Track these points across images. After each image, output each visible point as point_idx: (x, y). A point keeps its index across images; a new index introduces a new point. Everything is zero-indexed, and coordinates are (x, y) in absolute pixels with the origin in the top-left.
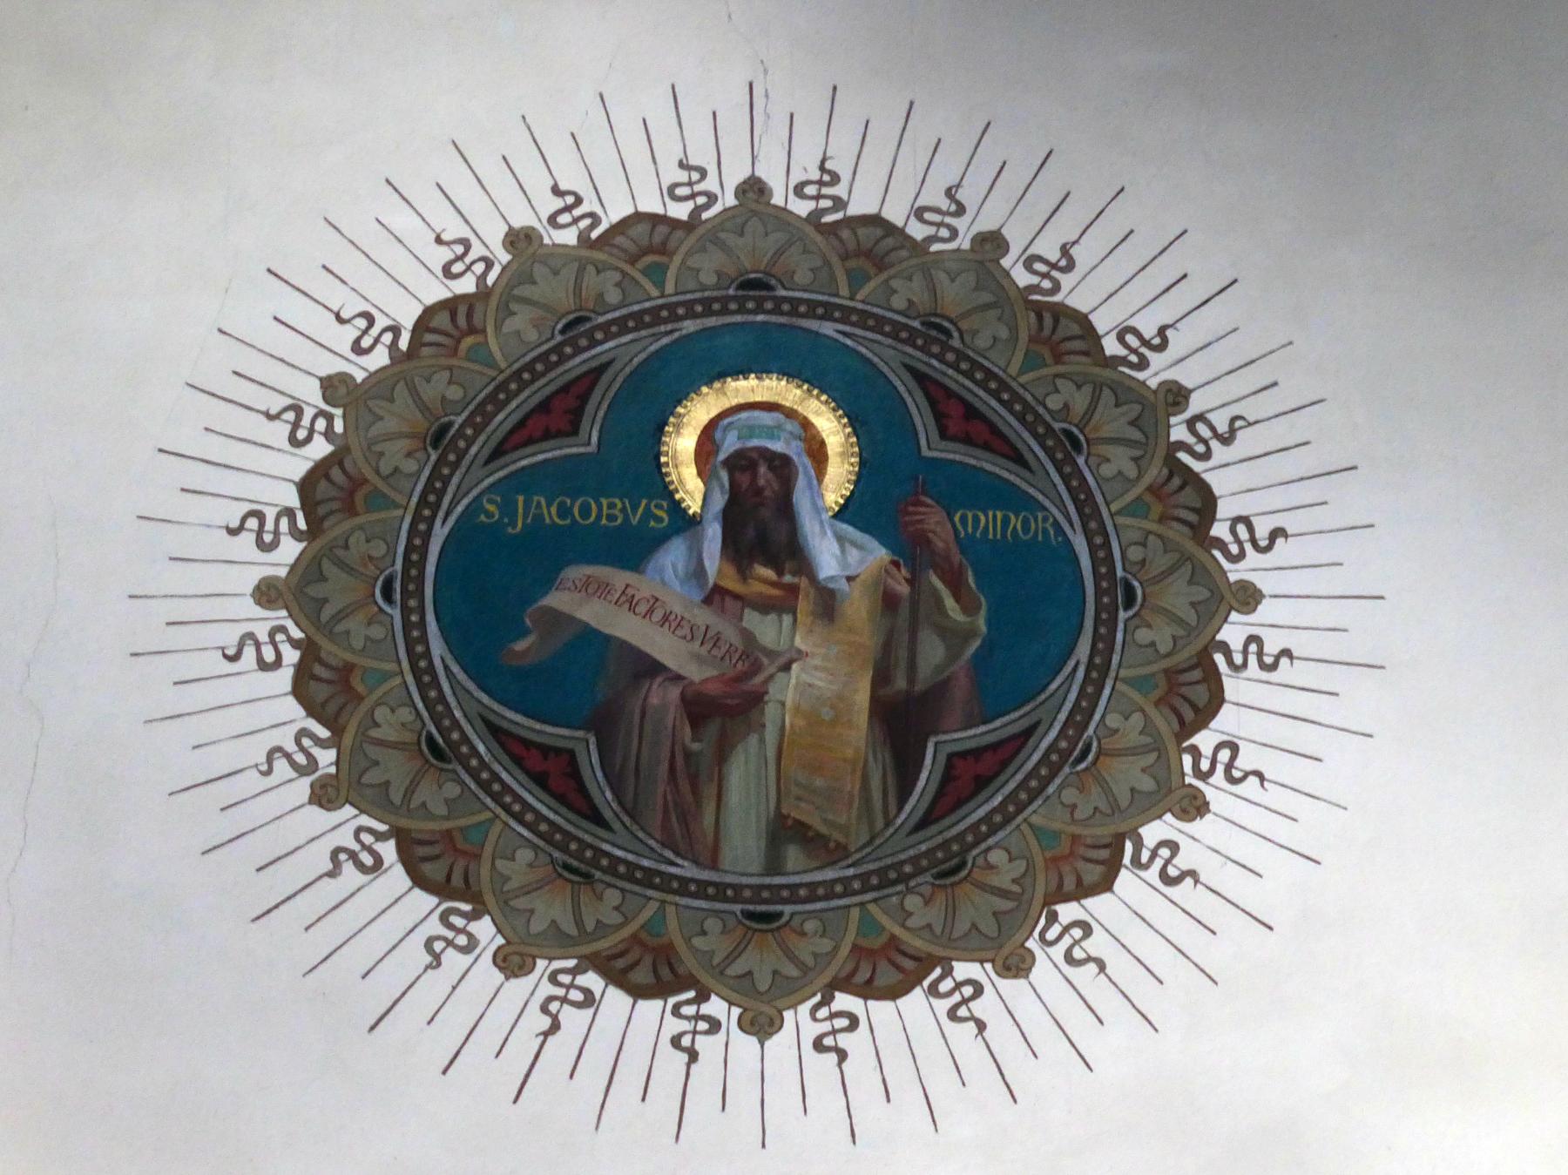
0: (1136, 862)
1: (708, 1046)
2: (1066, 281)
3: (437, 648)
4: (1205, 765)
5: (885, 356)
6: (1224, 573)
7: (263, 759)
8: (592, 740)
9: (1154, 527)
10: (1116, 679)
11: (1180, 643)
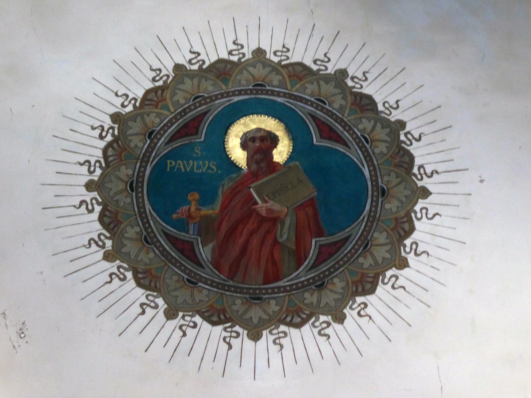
0: (136, 100)
1: (236, 343)
2: (144, 300)
3: (148, 207)
4: (111, 131)
5: (302, 110)
6: (99, 194)
7: (422, 138)
8: (199, 239)
9: (393, 169)
10: (378, 220)
11: (400, 209)
